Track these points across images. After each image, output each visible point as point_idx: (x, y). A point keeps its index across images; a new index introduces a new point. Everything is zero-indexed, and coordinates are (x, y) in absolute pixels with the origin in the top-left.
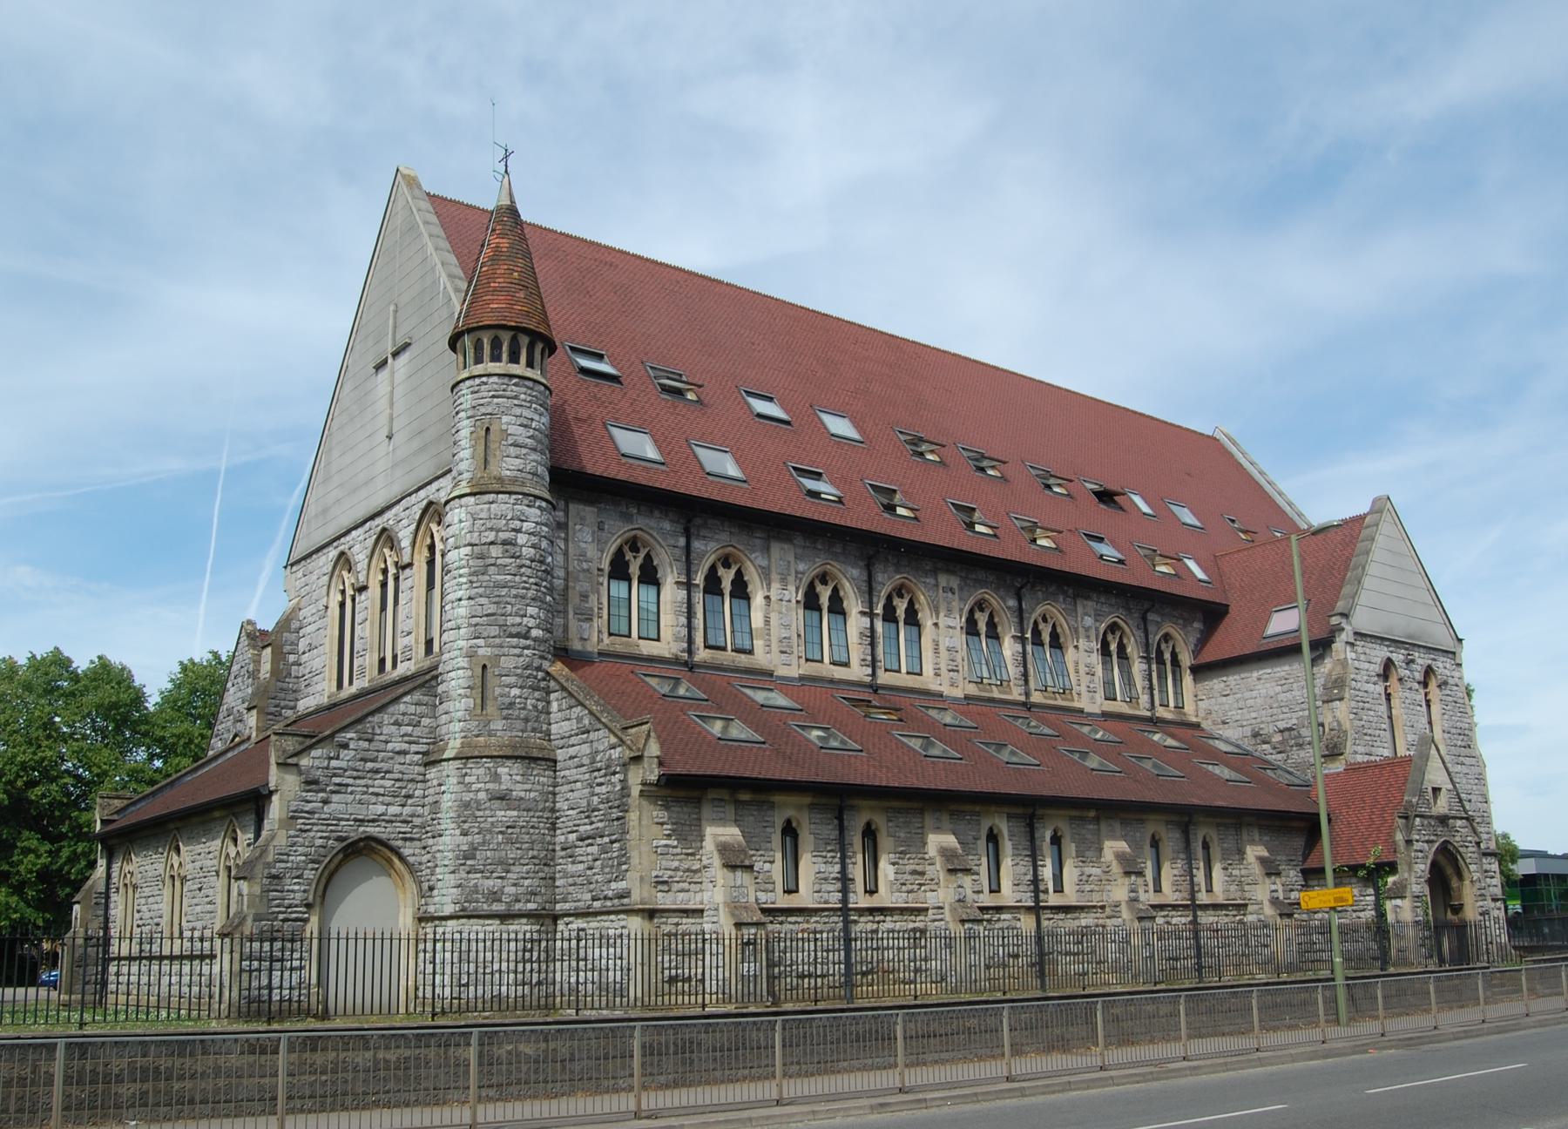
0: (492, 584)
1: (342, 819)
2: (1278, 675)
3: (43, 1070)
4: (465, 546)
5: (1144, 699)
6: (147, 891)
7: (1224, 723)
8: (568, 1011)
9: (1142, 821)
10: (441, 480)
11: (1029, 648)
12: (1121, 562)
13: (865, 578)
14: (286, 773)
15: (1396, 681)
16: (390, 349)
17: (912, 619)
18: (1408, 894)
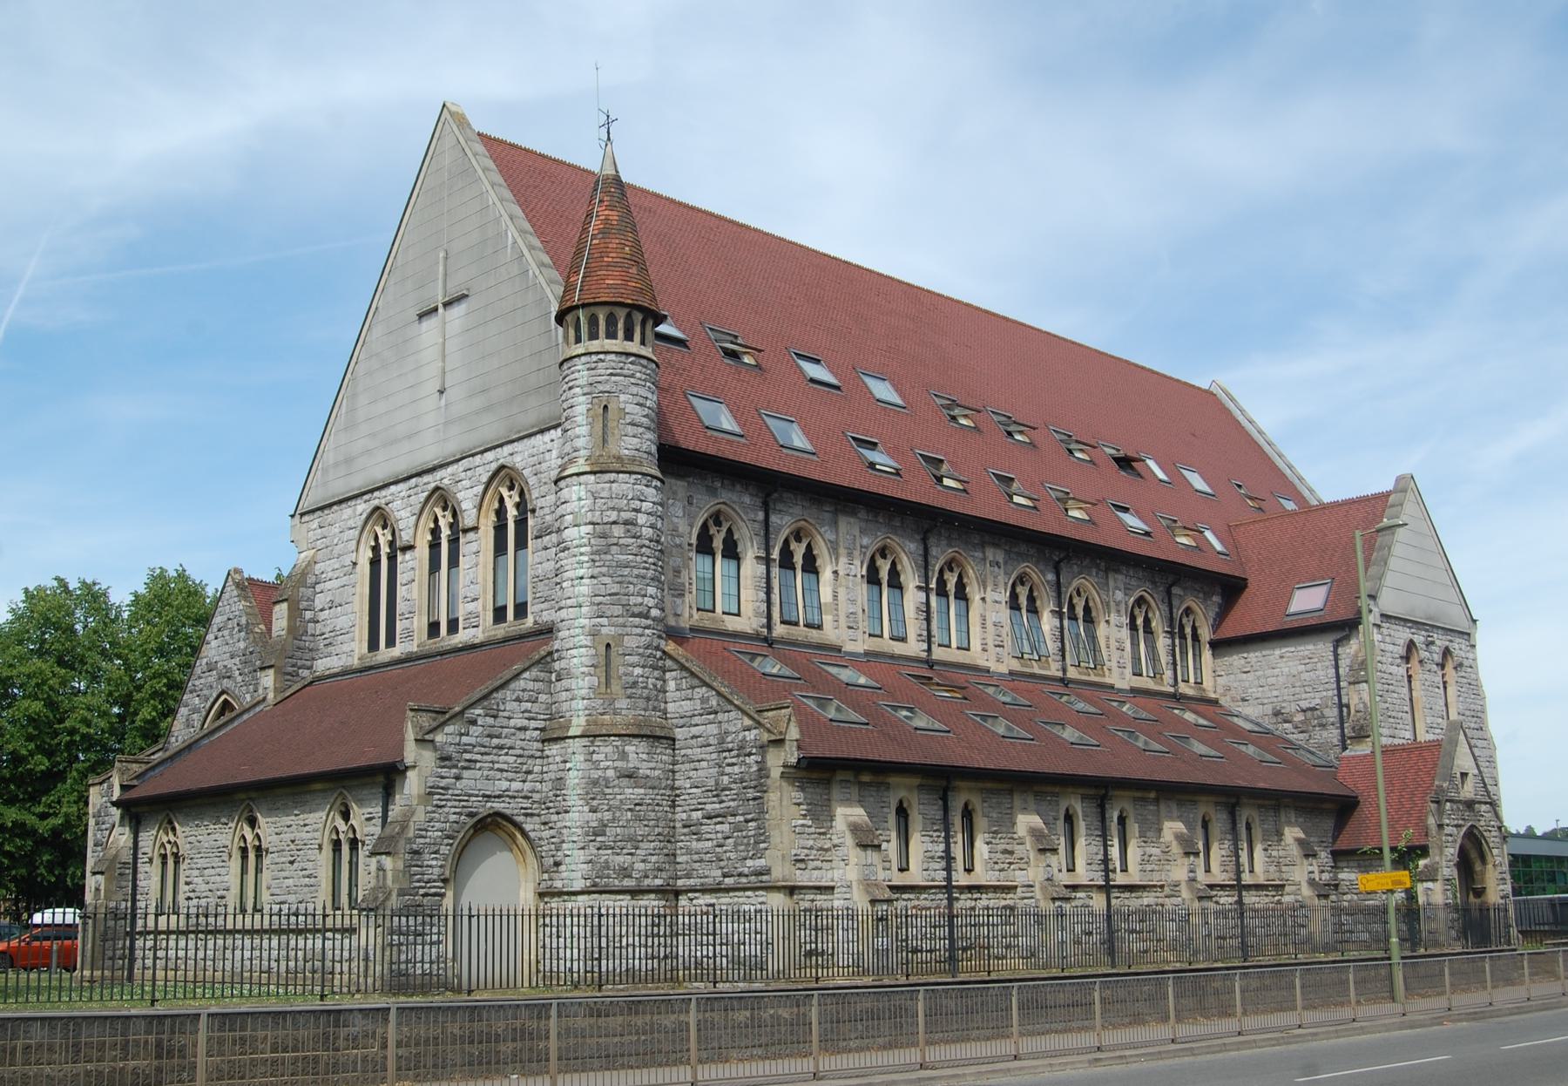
0: (615, 564)
1: (470, 795)
4: (586, 524)
6: (202, 863)
7: (1244, 700)
9: (1195, 802)
11: (1066, 622)
12: (1147, 534)
13: (921, 552)
15: (1417, 663)
16: (440, 299)
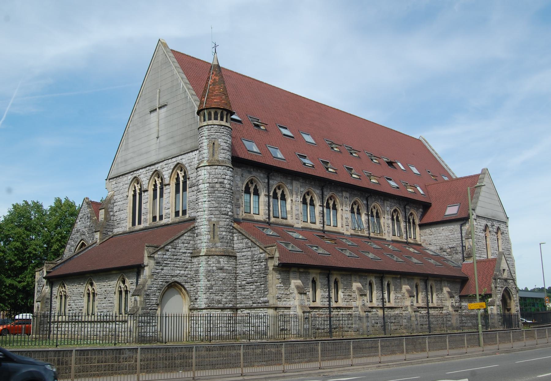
0: (216, 197)
3: (158, 356)
4: (207, 183)
6: (74, 298)
7: (430, 244)
8: (243, 340)
9: (413, 279)
11: (370, 218)
12: (398, 188)
13: (321, 193)
14: (150, 260)
16: (158, 106)
17: (335, 208)
18: (495, 305)
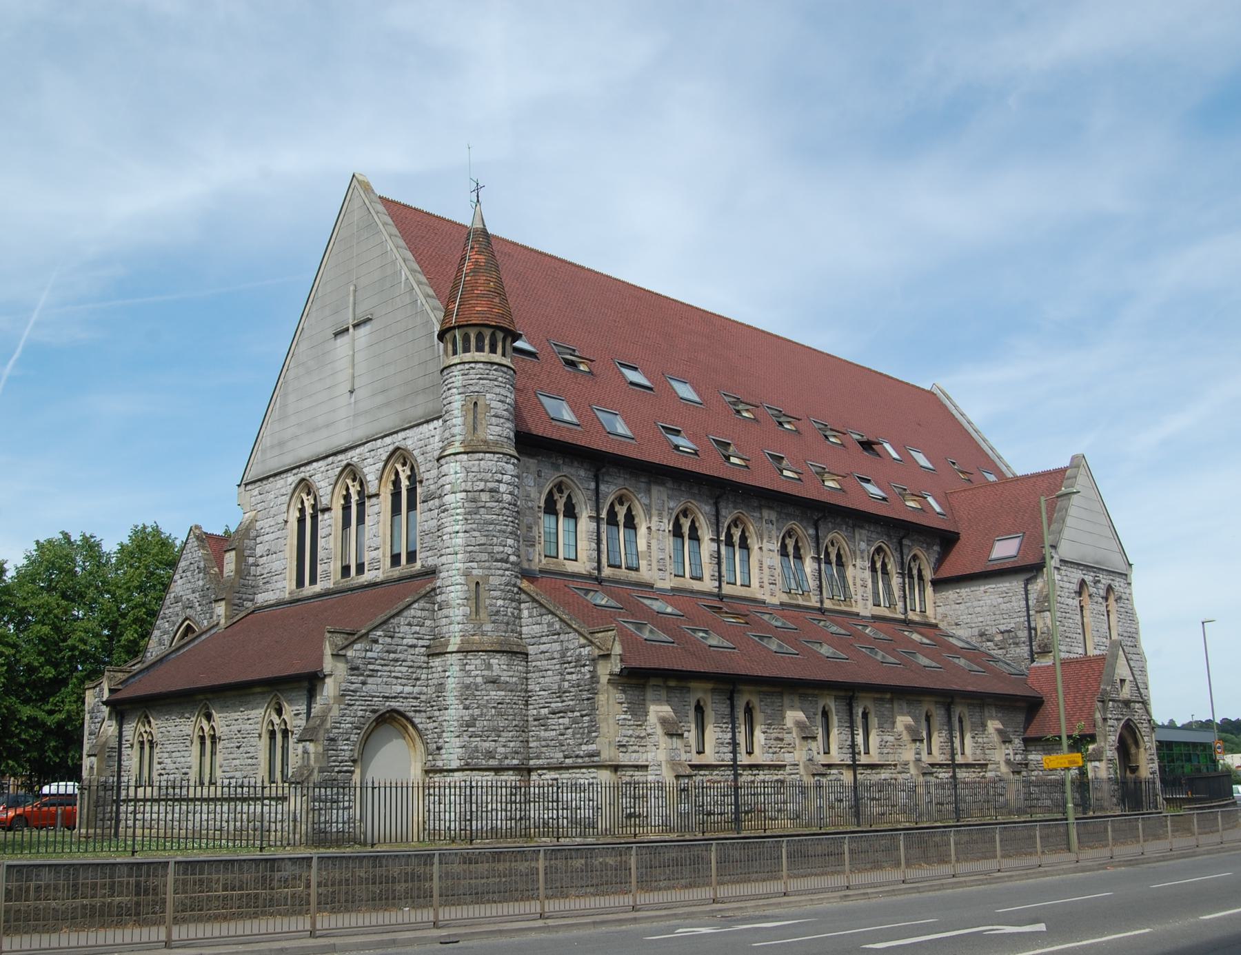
0: (482, 522)
2: (1000, 589)
4: (461, 492)
5: (900, 605)
6: (170, 748)
7: (957, 624)
9: (920, 702)
10: (407, 431)
12: (884, 499)
15: (1087, 597)
16: (351, 322)
17: (744, 545)
18: (1104, 758)
